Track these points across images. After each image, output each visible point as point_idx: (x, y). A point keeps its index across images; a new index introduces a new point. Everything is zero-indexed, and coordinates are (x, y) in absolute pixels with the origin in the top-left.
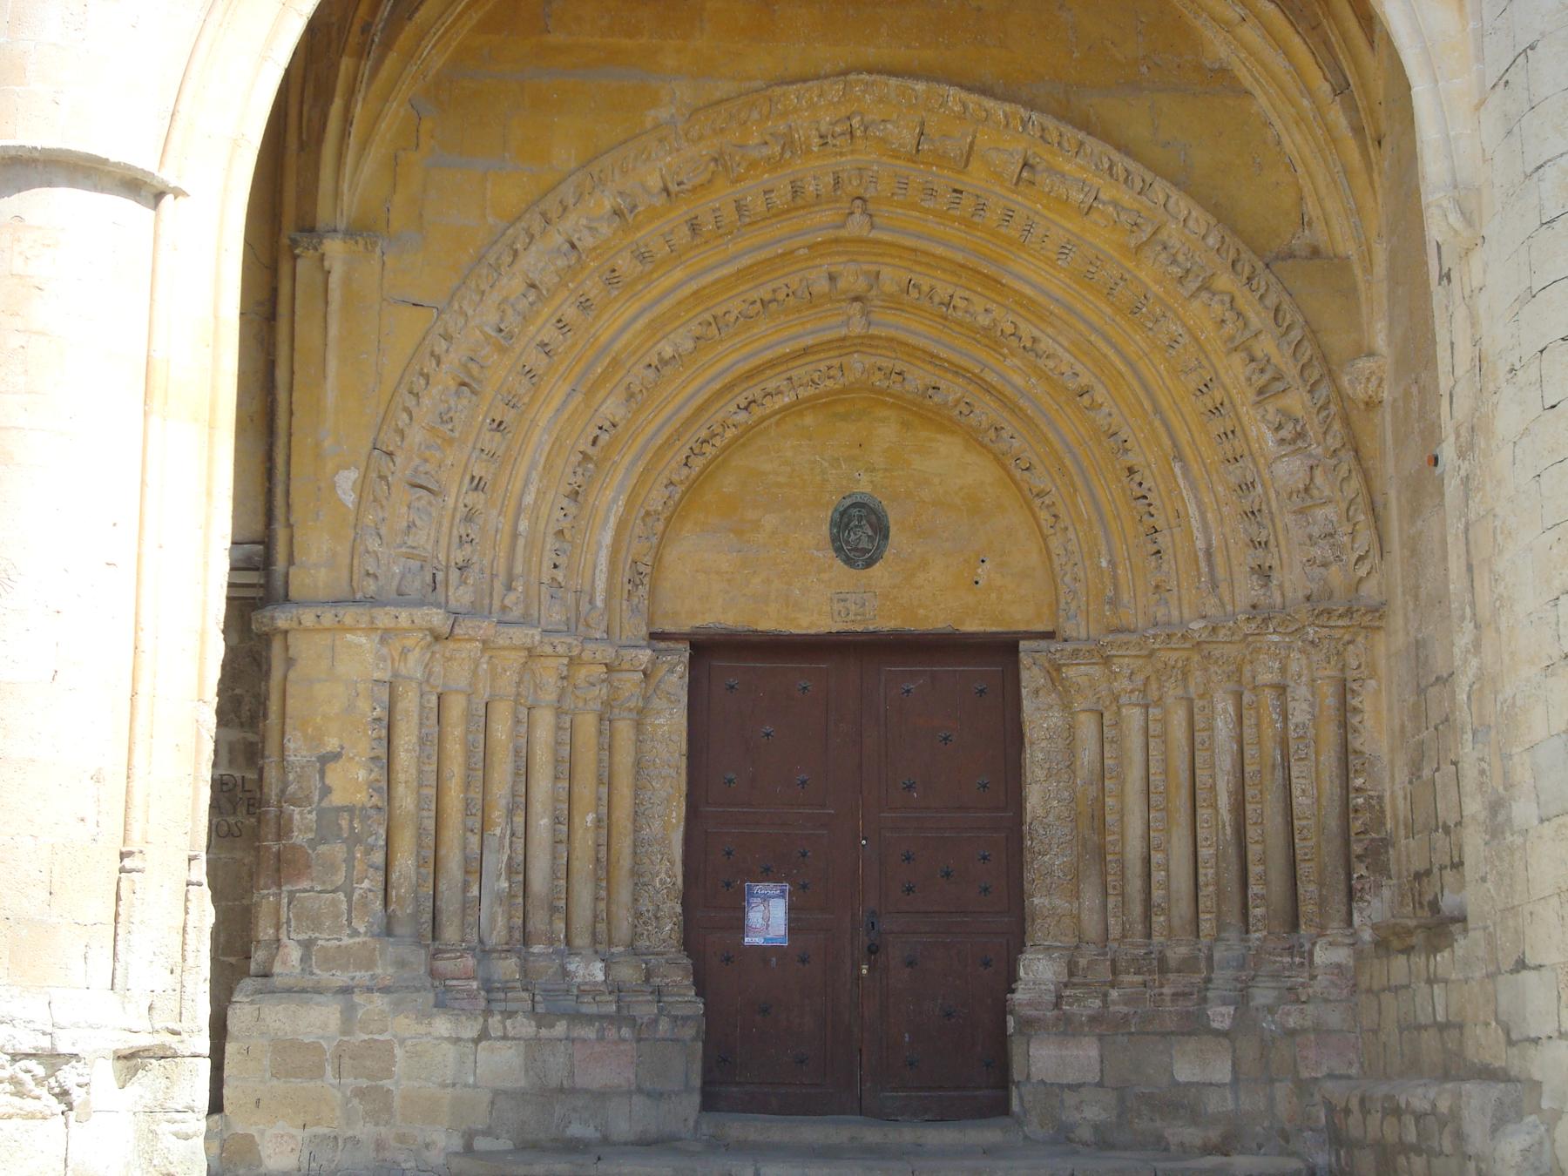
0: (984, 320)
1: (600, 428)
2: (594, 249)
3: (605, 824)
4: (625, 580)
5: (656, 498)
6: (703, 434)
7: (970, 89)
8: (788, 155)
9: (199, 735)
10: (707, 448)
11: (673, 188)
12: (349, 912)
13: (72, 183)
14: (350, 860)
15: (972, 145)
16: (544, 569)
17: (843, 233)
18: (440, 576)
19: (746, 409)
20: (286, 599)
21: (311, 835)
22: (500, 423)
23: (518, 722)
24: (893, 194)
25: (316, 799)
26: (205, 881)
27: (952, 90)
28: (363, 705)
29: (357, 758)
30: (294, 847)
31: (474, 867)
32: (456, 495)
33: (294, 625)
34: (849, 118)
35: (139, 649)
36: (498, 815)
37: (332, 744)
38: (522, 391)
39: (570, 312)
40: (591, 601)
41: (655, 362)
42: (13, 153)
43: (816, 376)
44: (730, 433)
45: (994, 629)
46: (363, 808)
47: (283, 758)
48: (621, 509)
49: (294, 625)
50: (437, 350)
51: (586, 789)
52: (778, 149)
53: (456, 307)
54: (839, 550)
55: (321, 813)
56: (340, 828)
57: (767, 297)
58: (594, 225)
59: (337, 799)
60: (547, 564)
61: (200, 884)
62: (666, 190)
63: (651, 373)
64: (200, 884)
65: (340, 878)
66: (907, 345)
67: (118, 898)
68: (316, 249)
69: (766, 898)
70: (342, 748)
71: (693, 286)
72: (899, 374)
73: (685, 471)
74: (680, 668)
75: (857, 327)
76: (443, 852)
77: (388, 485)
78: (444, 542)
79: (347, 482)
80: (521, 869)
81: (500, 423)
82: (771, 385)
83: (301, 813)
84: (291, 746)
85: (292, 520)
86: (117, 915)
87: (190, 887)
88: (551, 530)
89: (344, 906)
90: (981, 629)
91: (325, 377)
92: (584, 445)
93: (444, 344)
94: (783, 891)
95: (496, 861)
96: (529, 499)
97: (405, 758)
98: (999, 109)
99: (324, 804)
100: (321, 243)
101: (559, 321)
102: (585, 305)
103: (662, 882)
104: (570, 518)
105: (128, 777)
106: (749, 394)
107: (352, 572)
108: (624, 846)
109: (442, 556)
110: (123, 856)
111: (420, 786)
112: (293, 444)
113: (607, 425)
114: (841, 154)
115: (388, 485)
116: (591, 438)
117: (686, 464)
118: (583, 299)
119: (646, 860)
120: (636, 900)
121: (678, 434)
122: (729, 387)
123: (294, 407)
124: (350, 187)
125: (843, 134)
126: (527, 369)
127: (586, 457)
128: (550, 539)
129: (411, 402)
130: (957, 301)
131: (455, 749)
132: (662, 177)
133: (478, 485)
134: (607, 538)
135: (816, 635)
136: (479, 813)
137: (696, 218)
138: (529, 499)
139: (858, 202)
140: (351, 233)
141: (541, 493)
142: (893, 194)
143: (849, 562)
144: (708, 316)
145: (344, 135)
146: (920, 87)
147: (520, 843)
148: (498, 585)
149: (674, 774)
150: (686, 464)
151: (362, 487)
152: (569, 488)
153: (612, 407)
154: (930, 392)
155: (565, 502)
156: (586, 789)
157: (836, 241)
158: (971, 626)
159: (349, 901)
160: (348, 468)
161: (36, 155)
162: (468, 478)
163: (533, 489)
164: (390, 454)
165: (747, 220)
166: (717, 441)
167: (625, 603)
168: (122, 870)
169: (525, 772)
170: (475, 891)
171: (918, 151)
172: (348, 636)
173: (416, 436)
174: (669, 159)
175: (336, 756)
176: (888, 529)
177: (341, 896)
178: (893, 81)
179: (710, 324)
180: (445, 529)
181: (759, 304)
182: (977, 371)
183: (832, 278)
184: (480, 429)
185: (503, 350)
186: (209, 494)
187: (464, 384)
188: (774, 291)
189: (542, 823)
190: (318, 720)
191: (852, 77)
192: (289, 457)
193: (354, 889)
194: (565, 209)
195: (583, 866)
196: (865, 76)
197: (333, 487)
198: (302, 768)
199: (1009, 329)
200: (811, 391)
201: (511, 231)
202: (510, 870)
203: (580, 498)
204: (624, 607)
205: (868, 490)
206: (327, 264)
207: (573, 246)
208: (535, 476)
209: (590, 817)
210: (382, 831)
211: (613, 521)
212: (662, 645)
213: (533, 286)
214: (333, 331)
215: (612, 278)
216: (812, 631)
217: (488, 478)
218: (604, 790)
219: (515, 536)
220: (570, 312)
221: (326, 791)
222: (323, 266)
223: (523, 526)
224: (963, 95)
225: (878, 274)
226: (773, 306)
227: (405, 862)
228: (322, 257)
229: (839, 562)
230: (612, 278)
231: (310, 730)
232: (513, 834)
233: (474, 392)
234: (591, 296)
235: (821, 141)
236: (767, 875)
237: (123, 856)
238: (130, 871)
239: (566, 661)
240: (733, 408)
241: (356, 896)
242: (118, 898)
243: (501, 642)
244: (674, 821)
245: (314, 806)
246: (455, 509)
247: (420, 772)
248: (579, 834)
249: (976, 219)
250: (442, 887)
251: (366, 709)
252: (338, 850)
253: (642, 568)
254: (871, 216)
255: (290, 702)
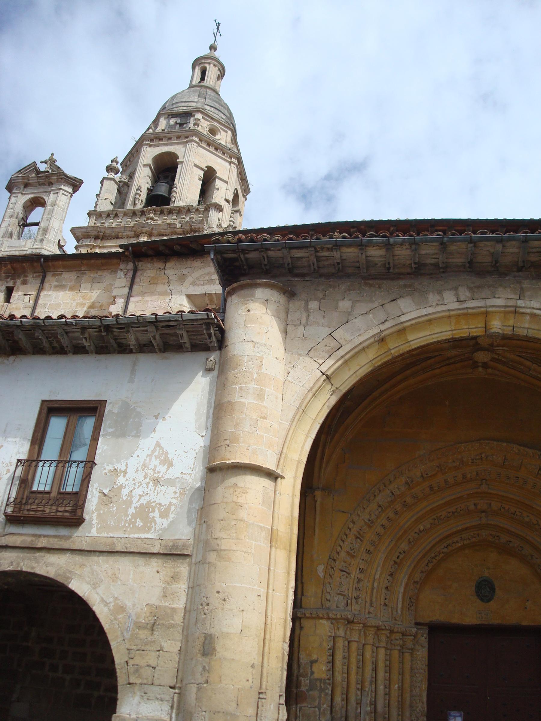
0: (527, 519)
1: (400, 553)
2: (399, 495)
3: (401, 689)
4: (407, 604)
5: (417, 576)
6: (433, 555)
7: (520, 445)
8: (461, 465)
9: (283, 654)
10: (434, 560)
11: (425, 476)
12: (319, 715)
13: (252, 474)
14: (320, 697)
15: (522, 463)
16: (382, 600)
17: (479, 490)
18: (349, 601)
19: (447, 547)
20: (301, 607)
21: (307, 688)
22: (369, 551)
23: (373, 652)
24: (496, 478)
25: (309, 675)
26: (284, 703)
27: (515, 446)
28: (325, 644)
29: (323, 662)
30: (302, 691)
31: (359, 703)
32: (355, 574)
33: (303, 616)
34: (481, 454)
35: (267, 624)
36: (367, 684)
37: (315, 657)
38: (376, 541)
39: (391, 515)
40: (397, 611)
41: (418, 531)
42: (235, 464)
43: (470, 537)
44: (441, 555)
45: (532, 624)
46: (324, 680)
47: (299, 661)
48: (406, 580)
49: (303, 616)
50: (350, 527)
51: (395, 676)
52: (458, 464)
53: (356, 513)
54: (478, 596)
55: (310, 680)
56: (317, 686)
57: (454, 511)
58: (400, 487)
59: (316, 676)
60: (383, 598)
61: (283, 704)
62: (422, 476)
63: (416, 535)
64: (283, 704)
65: (316, 703)
66: (500, 527)
67: (258, 708)
68: (312, 494)
69: (455, 717)
70: (318, 658)
71: (430, 507)
72: (497, 536)
73: (427, 568)
74: (425, 635)
75: (484, 521)
76: (349, 695)
77: (334, 570)
78: (350, 590)
79: (321, 569)
80: (374, 703)
81: (369, 551)
82: (455, 540)
83: (304, 680)
84: (301, 657)
85: (303, 581)
86: (257, 713)
87: (280, 705)
88: (384, 586)
89: (318, 713)
90: (528, 624)
91: (314, 535)
92: (395, 558)
93: (352, 525)
94: (461, 714)
95: (366, 700)
96: (377, 576)
97: (338, 663)
98: (530, 451)
99: (312, 677)
100: (314, 492)
101: (388, 518)
102: (396, 513)
103: (420, 710)
104: (390, 583)
105: (262, 667)
106: (448, 542)
107: (322, 599)
108: (407, 696)
109: (350, 595)
110: (260, 693)
111: (343, 673)
112: (304, 556)
113: (402, 552)
114: (478, 465)
115: (334, 570)
116: (397, 556)
117: (427, 566)
118: (395, 511)
119: (414, 702)
120: (411, 716)
121: (424, 556)
122: (441, 540)
123: (305, 544)
124: (323, 475)
125: (479, 459)
126: (378, 533)
127: (395, 562)
128: (384, 590)
129: (341, 543)
130: (518, 513)
131: (353, 660)
132: (421, 472)
133: (361, 571)
134: (402, 590)
135: (472, 625)
136: (361, 683)
137: (432, 485)
138: (377, 576)
139: (484, 481)
140: (323, 489)
141: (381, 574)
142: (496, 478)
143: (482, 600)
144: (434, 517)
145: (322, 459)
146: (504, 444)
147: (373, 694)
148: (368, 604)
149: (424, 672)
150: (427, 566)
151: (325, 571)
152: (390, 573)
153: (404, 546)
154: (508, 543)
155: (389, 578)
156: (395, 676)
157: (477, 493)
158: (525, 623)
159: (320, 711)
160: (321, 565)
161: (242, 465)
162: (358, 569)
163: (379, 572)
164: (335, 560)
165: (448, 486)
166: (437, 558)
167: (407, 612)
168: (259, 698)
169: (375, 670)
170: (359, 710)
171: (504, 464)
172: (320, 620)
173: (343, 554)
174: (423, 467)
175: (316, 661)
176: (495, 589)
177: (317, 709)
178: (495, 443)
179: (435, 519)
180: (351, 585)
181: (451, 513)
182: (524, 536)
183: (475, 505)
184: (362, 553)
185: (370, 527)
186: (288, 573)
187: (357, 538)
188: (456, 509)
189: (381, 688)
190: (310, 648)
191: (482, 441)
192: (302, 560)
193: (321, 707)
194: (391, 482)
195: (394, 703)
196: (486, 441)
197: (316, 570)
198: (305, 664)
199: (535, 522)
200: (468, 542)
201: (373, 489)
202: (371, 704)
203: (393, 576)
204: (407, 613)
205: (488, 575)
206: (316, 499)
207: (393, 494)
208: (379, 568)
209: (396, 686)
210: (330, 688)
211: (403, 584)
212: (419, 627)
213: (380, 506)
214: (317, 520)
215: (405, 505)
216: (470, 624)
217: (365, 568)
218: (400, 677)
219: (373, 588)
220: (391, 515)
221: (312, 673)
222: (314, 499)
223: (376, 585)
224: (518, 447)
225: (490, 504)
226: (456, 514)
227: (338, 699)
228: (314, 496)
229: (478, 600)
230: (405, 505)
231: (307, 652)
232: (372, 691)
233: (361, 540)
234: (398, 510)
235: (472, 461)
236: (455, 709)
237: (260, 693)
238: (262, 699)
239: (389, 632)
240: (442, 547)
241: (322, 710)
242: (258, 708)
243: (368, 624)
244: (424, 688)
245: (309, 678)
246: (354, 579)
247: (343, 668)
248: (392, 692)
249: (523, 486)
250: (349, 708)
251: (327, 645)
252: (316, 693)
253: (413, 601)
254: (488, 485)
255: (301, 642)
